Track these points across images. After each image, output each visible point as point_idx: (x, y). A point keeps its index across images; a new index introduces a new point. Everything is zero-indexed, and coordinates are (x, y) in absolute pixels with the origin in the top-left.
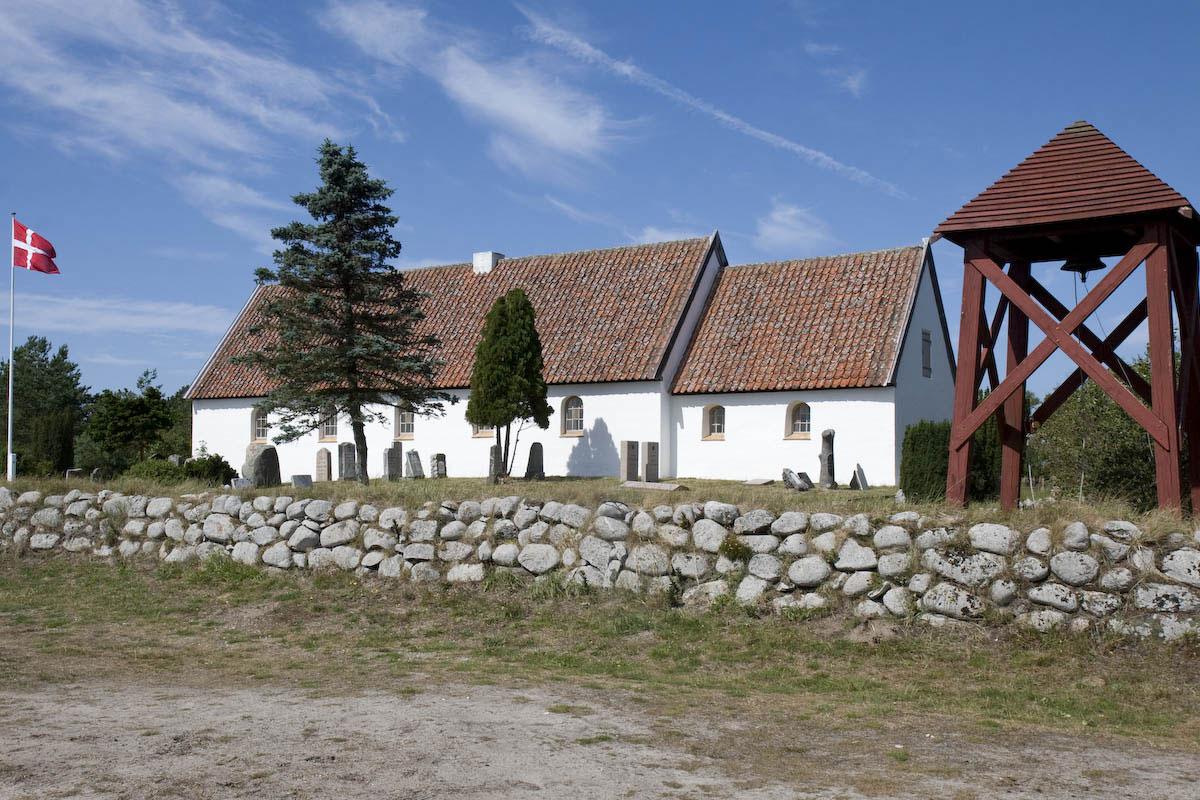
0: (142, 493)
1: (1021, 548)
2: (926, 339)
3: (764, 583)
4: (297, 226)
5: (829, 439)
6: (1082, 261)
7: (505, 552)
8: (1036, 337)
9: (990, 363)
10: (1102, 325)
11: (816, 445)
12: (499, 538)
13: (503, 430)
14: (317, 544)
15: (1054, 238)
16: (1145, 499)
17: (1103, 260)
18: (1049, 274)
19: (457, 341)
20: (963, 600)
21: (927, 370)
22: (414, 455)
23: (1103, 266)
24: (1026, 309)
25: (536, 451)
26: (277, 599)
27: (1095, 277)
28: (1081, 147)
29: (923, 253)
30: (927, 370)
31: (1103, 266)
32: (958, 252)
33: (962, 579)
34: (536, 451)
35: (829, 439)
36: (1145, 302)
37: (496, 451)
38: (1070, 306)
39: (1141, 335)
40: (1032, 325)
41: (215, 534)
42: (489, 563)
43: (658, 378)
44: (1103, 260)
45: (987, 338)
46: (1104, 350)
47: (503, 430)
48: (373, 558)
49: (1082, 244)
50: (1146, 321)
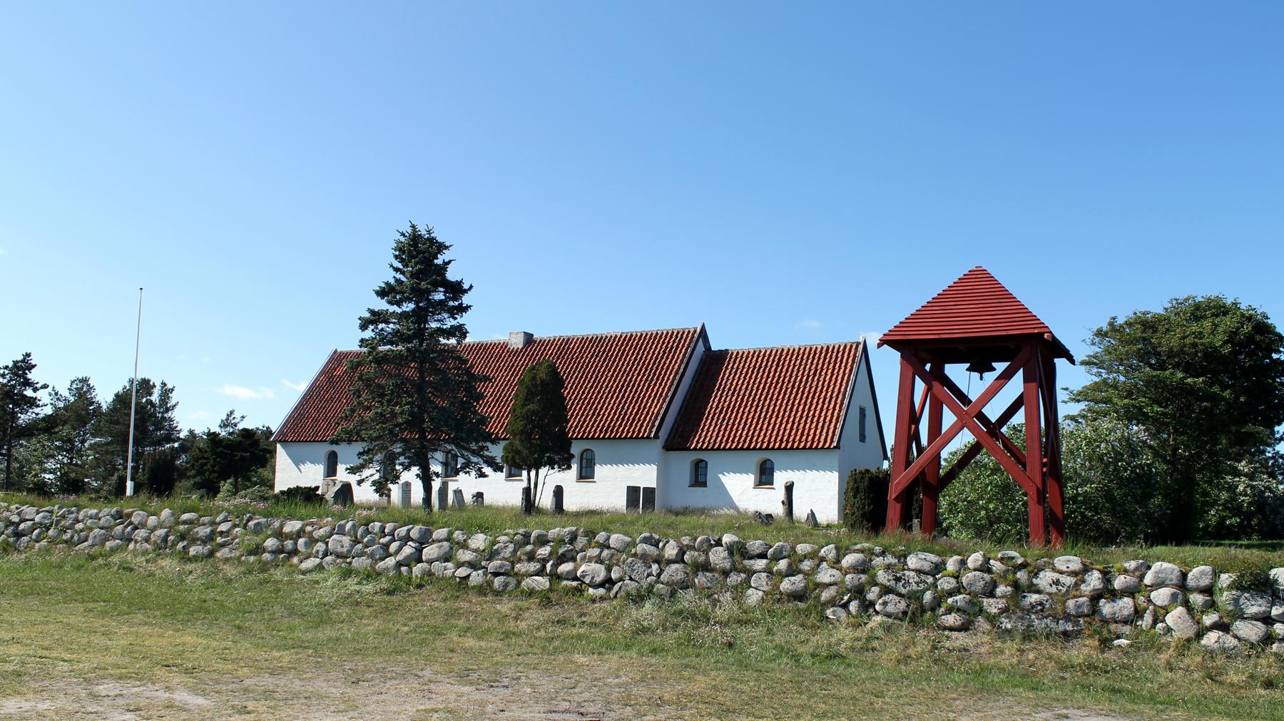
0: (277, 516)
1: (938, 568)
2: (862, 412)
3: (761, 593)
4: (372, 312)
5: (789, 489)
6: (980, 366)
7: (565, 567)
8: (949, 418)
9: (916, 437)
10: (993, 411)
11: (780, 494)
12: (562, 559)
13: (533, 473)
14: (420, 561)
15: (961, 348)
16: (1021, 539)
17: (994, 364)
18: (957, 372)
19: (499, 406)
20: (902, 605)
21: (863, 438)
22: (458, 493)
23: (994, 369)
24: (940, 396)
25: (559, 492)
26: (862, 551)
27: (990, 377)
28: (979, 286)
29: (861, 347)
30: (863, 438)
31: (994, 369)
32: (896, 356)
33: (903, 591)
34: (559, 492)
35: (789, 489)
36: (1021, 396)
37: (527, 491)
38: (973, 397)
39: (1019, 418)
40: (946, 409)
41: (339, 549)
42: (555, 577)
43: (656, 436)
44: (994, 364)
45: (915, 419)
46: (993, 429)
47: (533, 473)
48: (462, 572)
49: (979, 354)
50: (1023, 409)
